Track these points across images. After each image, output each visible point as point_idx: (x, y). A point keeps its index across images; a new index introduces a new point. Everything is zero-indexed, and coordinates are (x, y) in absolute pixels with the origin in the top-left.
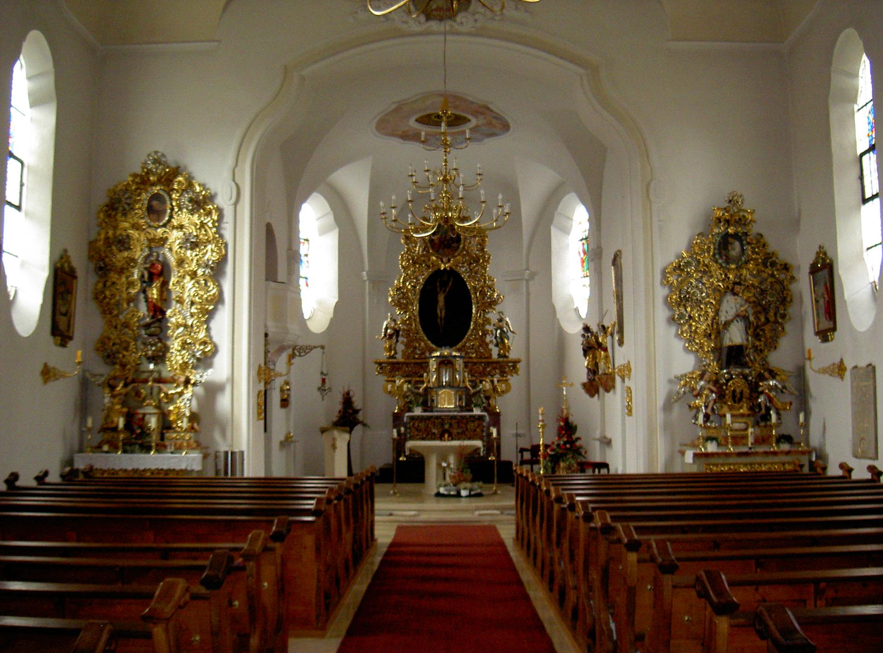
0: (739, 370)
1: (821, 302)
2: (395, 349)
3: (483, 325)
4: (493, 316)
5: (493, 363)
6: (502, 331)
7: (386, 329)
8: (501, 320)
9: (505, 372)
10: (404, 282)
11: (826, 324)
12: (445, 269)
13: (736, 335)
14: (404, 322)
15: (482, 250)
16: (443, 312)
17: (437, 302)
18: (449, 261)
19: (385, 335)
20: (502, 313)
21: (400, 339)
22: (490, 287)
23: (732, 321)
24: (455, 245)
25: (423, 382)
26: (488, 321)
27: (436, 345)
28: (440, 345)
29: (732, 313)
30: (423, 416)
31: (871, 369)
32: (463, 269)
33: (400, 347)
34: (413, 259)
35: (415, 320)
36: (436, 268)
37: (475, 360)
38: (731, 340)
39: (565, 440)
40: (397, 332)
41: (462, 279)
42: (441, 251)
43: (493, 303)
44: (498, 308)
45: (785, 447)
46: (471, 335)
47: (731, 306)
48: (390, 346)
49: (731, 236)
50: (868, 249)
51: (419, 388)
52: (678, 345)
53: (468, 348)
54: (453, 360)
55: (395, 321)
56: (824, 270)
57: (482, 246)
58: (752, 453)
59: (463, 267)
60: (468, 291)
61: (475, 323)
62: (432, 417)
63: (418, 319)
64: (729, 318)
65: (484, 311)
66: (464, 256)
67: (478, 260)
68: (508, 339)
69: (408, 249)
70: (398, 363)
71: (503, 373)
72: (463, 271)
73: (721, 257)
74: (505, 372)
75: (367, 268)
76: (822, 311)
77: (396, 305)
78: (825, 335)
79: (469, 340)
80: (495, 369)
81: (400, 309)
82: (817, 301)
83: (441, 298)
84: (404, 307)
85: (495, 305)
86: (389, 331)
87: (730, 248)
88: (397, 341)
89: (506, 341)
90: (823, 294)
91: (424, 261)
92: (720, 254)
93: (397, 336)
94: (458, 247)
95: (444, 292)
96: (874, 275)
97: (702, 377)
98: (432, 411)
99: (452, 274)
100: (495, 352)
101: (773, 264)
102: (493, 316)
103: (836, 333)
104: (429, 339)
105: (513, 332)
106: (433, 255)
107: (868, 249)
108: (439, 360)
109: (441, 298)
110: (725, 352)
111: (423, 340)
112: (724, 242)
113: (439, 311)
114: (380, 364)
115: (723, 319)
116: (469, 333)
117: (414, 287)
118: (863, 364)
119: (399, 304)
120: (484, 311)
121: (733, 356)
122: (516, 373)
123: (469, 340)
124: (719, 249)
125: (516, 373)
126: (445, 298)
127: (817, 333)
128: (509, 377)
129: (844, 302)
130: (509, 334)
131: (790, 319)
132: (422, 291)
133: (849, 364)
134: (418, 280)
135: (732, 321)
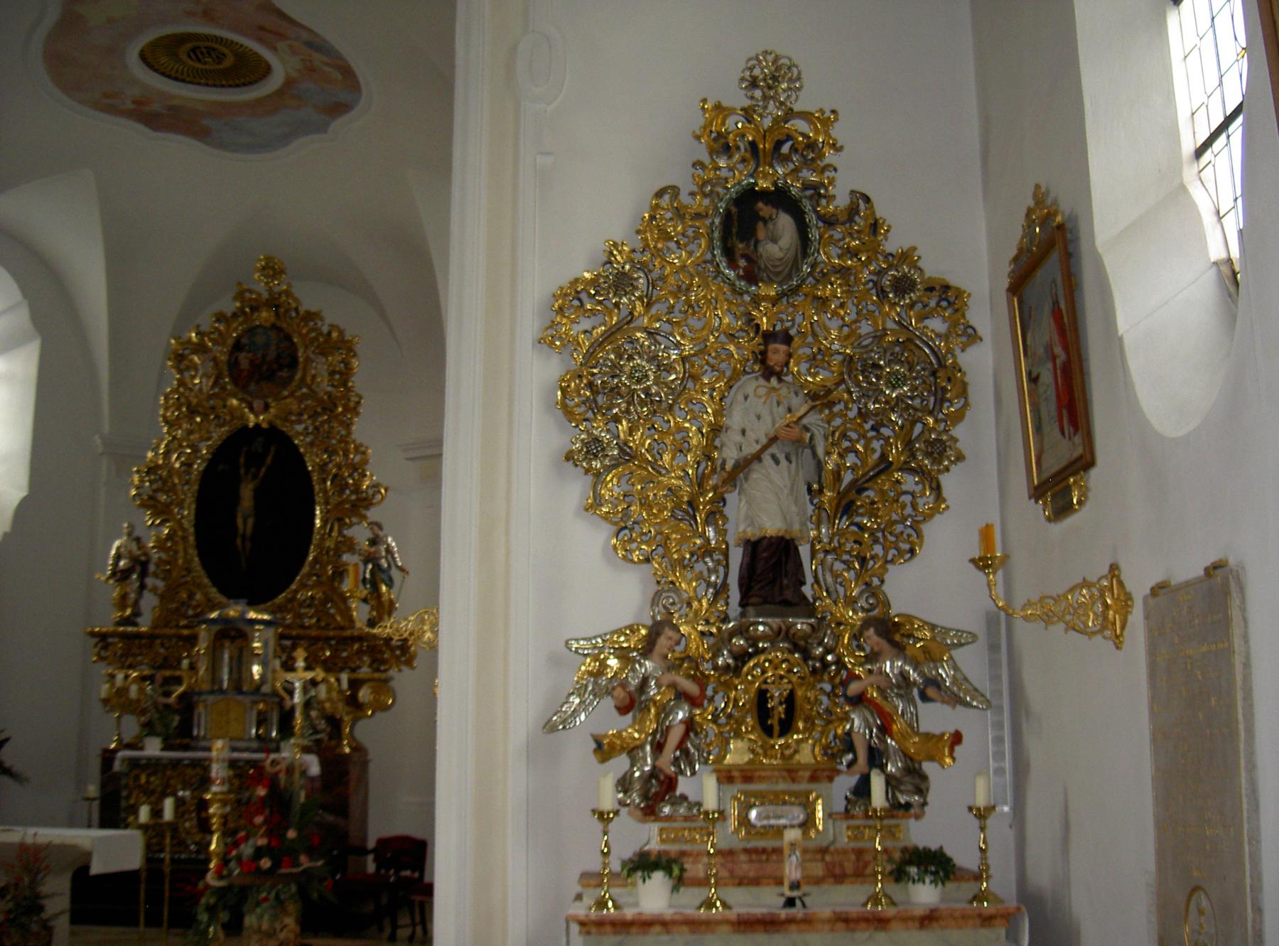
0: (775, 622)
1: (1047, 377)
2: (136, 604)
3: (338, 552)
4: (360, 533)
5: (353, 639)
6: (377, 567)
7: (118, 557)
8: (374, 542)
9: (384, 662)
10: (167, 454)
11: (1063, 450)
12: (257, 426)
13: (769, 504)
14: (160, 545)
15: (345, 384)
16: (251, 521)
17: (236, 499)
18: (267, 407)
19: (114, 574)
20: (380, 527)
21: (150, 581)
22: (354, 468)
23: (757, 457)
24: (284, 373)
25: (179, 681)
26: (349, 545)
27: (222, 591)
28: (233, 591)
29: (760, 432)
30: (158, 759)
31: (1220, 583)
32: (300, 428)
33: (149, 603)
34: (189, 405)
35: (184, 538)
36: (238, 424)
37: (313, 633)
38: (751, 520)
39: (262, 842)
40: (140, 565)
41: (296, 447)
42: (252, 387)
43: (362, 503)
44: (373, 514)
45: (925, 894)
46: (309, 575)
47: (754, 413)
48: (124, 597)
49: (764, 194)
50: (1199, 152)
51: (167, 694)
52: (591, 540)
53: (301, 605)
54: (247, 629)
55: (138, 540)
56: (1052, 265)
57: (343, 375)
58: (791, 921)
59: (299, 422)
60: (308, 475)
61: (320, 546)
62: (179, 761)
63: (192, 539)
64: (751, 449)
65: (340, 520)
66: (305, 397)
67: (337, 407)
68: (390, 584)
69: (181, 383)
70: (139, 636)
71: (378, 663)
72: (300, 434)
73: (732, 264)
74: (384, 662)
75: (106, 428)
76: (1049, 409)
77: (144, 506)
78: (1058, 489)
79: (303, 589)
80: (360, 652)
81: (155, 515)
82: (1034, 380)
83: (247, 493)
84: (162, 511)
85: (367, 508)
86: (122, 563)
87: (761, 233)
88: (142, 587)
89: (384, 588)
90: (1049, 347)
91: (213, 408)
92: (729, 253)
93: (144, 574)
94: (291, 378)
95: (255, 476)
96: (1222, 238)
97: (648, 647)
98: (186, 748)
99: (275, 437)
100: (360, 613)
101: (903, 286)
102: (360, 533)
103: (1093, 473)
104: (215, 584)
105: (401, 569)
106: (235, 396)
107: (1199, 152)
108: (216, 628)
109: (247, 493)
110: (737, 557)
111: (199, 586)
112: (741, 220)
113: (240, 521)
114: (103, 637)
115: (730, 455)
116: (306, 569)
117: (188, 465)
118: (1189, 568)
119: (149, 502)
120: (340, 520)
121: (770, 571)
122: (409, 663)
123: (303, 586)
124: (725, 238)
125: (409, 663)
126: (258, 494)
127: (1037, 493)
128: (393, 672)
129: (1114, 342)
130: (395, 573)
131: (960, 458)
132: (206, 476)
133: (1139, 583)
134: (196, 451)
135: (757, 457)
